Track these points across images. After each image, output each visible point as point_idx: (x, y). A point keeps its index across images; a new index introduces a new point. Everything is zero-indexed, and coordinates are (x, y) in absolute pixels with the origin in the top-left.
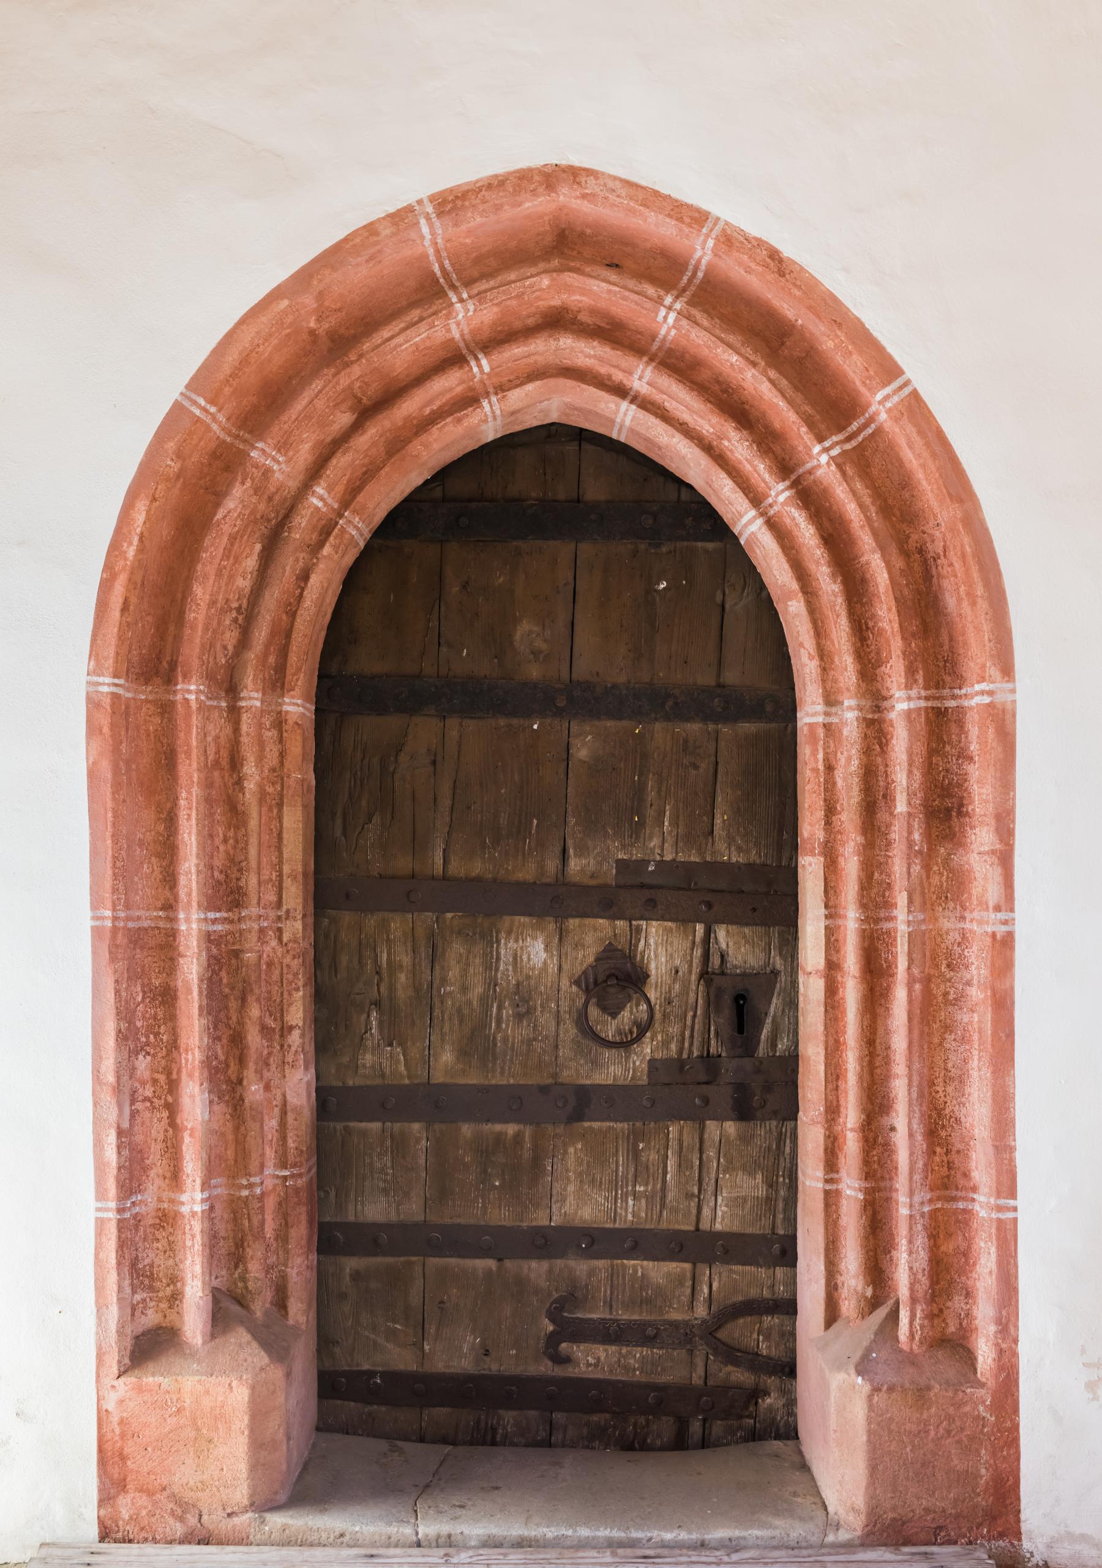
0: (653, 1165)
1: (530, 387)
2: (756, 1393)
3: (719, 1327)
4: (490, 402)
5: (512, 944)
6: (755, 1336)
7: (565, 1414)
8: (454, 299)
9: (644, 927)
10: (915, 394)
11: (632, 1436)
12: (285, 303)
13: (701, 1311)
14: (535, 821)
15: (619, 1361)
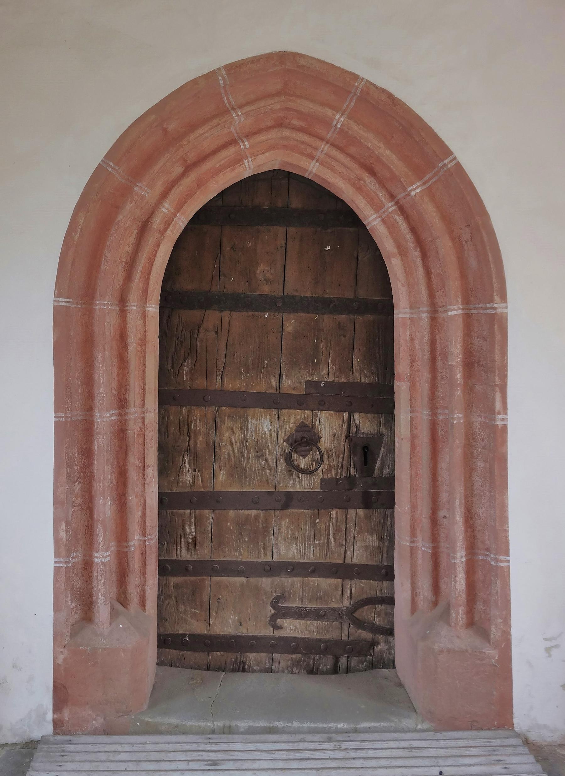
0: (323, 530)
1: (267, 154)
2: (373, 644)
3: (355, 611)
4: (248, 162)
5: (254, 422)
6: (373, 615)
7: (279, 654)
8: (234, 115)
9: (319, 413)
10: (458, 162)
11: (312, 665)
12: (153, 117)
13: (346, 603)
14: (266, 362)
15: (306, 628)
